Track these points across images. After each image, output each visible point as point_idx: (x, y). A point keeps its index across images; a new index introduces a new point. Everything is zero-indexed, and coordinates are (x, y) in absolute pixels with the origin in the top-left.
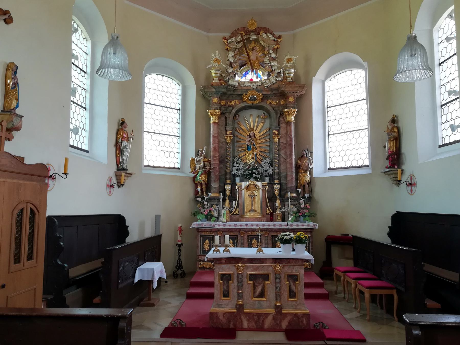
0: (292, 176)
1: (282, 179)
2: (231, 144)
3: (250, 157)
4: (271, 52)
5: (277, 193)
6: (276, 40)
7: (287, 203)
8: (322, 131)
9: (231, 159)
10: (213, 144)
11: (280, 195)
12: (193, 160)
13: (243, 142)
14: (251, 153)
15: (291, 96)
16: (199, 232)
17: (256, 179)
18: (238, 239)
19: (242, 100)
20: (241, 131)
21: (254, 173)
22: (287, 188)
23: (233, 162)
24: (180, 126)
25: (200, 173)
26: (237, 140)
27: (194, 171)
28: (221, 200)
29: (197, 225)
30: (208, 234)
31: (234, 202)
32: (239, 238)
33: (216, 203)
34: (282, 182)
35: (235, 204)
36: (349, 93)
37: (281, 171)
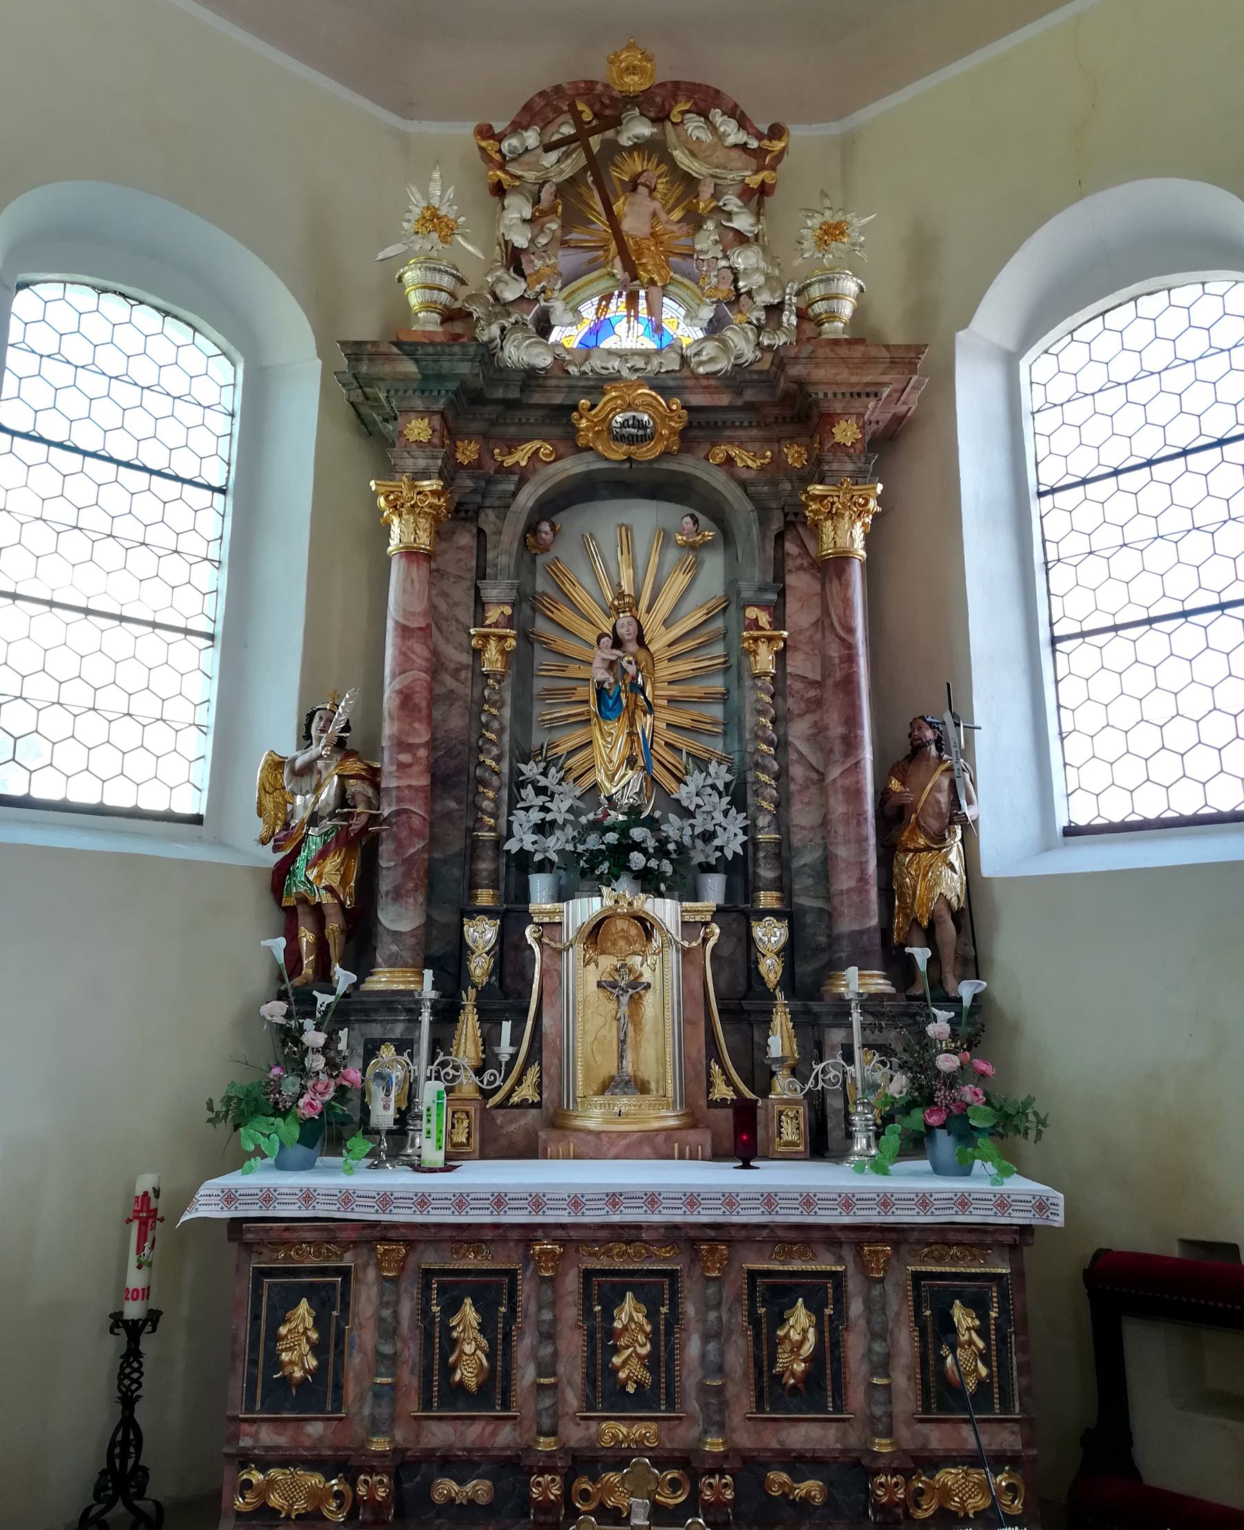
0: (862, 866)
1: (802, 883)
2: (507, 682)
3: (616, 758)
4: (732, 202)
5: (770, 968)
6: (754, 144)
7: (836, 1036)
8: (1013, 620)
9: (505, 767)
10: (401, 670)
11: (789, 981)
12: (277, 765)
13: (574, 671)
14: (617, 729)
15: (845, 415)
16: (248, 1246)
17: (648, 882)
18: (521, 1298)
19: (571, 442)
20: (565, 615)
21: (638, 847)
22: (833, 940)
23: (518, 783)
24: (220, 579)
25: (315, 843)
26: (542, 659)
27: (286, 838)
28: (426, 1017)
29: (230, 1197)
30: (312, 1262)
31: (507, 1026)
32: (526, 1289)
33: (398, 1030)
34: (804, 901)
35: (516, 1041)
36: (1163, 409)
37: (796, 840)
